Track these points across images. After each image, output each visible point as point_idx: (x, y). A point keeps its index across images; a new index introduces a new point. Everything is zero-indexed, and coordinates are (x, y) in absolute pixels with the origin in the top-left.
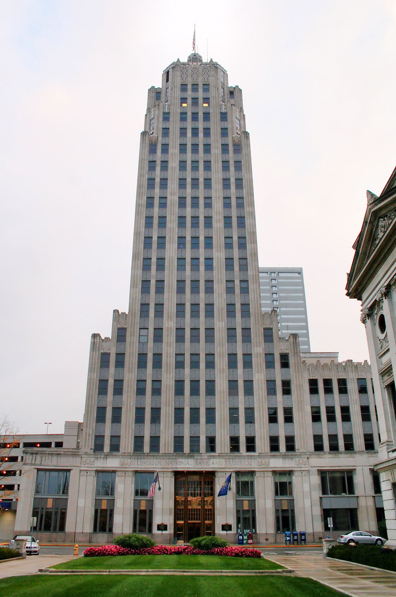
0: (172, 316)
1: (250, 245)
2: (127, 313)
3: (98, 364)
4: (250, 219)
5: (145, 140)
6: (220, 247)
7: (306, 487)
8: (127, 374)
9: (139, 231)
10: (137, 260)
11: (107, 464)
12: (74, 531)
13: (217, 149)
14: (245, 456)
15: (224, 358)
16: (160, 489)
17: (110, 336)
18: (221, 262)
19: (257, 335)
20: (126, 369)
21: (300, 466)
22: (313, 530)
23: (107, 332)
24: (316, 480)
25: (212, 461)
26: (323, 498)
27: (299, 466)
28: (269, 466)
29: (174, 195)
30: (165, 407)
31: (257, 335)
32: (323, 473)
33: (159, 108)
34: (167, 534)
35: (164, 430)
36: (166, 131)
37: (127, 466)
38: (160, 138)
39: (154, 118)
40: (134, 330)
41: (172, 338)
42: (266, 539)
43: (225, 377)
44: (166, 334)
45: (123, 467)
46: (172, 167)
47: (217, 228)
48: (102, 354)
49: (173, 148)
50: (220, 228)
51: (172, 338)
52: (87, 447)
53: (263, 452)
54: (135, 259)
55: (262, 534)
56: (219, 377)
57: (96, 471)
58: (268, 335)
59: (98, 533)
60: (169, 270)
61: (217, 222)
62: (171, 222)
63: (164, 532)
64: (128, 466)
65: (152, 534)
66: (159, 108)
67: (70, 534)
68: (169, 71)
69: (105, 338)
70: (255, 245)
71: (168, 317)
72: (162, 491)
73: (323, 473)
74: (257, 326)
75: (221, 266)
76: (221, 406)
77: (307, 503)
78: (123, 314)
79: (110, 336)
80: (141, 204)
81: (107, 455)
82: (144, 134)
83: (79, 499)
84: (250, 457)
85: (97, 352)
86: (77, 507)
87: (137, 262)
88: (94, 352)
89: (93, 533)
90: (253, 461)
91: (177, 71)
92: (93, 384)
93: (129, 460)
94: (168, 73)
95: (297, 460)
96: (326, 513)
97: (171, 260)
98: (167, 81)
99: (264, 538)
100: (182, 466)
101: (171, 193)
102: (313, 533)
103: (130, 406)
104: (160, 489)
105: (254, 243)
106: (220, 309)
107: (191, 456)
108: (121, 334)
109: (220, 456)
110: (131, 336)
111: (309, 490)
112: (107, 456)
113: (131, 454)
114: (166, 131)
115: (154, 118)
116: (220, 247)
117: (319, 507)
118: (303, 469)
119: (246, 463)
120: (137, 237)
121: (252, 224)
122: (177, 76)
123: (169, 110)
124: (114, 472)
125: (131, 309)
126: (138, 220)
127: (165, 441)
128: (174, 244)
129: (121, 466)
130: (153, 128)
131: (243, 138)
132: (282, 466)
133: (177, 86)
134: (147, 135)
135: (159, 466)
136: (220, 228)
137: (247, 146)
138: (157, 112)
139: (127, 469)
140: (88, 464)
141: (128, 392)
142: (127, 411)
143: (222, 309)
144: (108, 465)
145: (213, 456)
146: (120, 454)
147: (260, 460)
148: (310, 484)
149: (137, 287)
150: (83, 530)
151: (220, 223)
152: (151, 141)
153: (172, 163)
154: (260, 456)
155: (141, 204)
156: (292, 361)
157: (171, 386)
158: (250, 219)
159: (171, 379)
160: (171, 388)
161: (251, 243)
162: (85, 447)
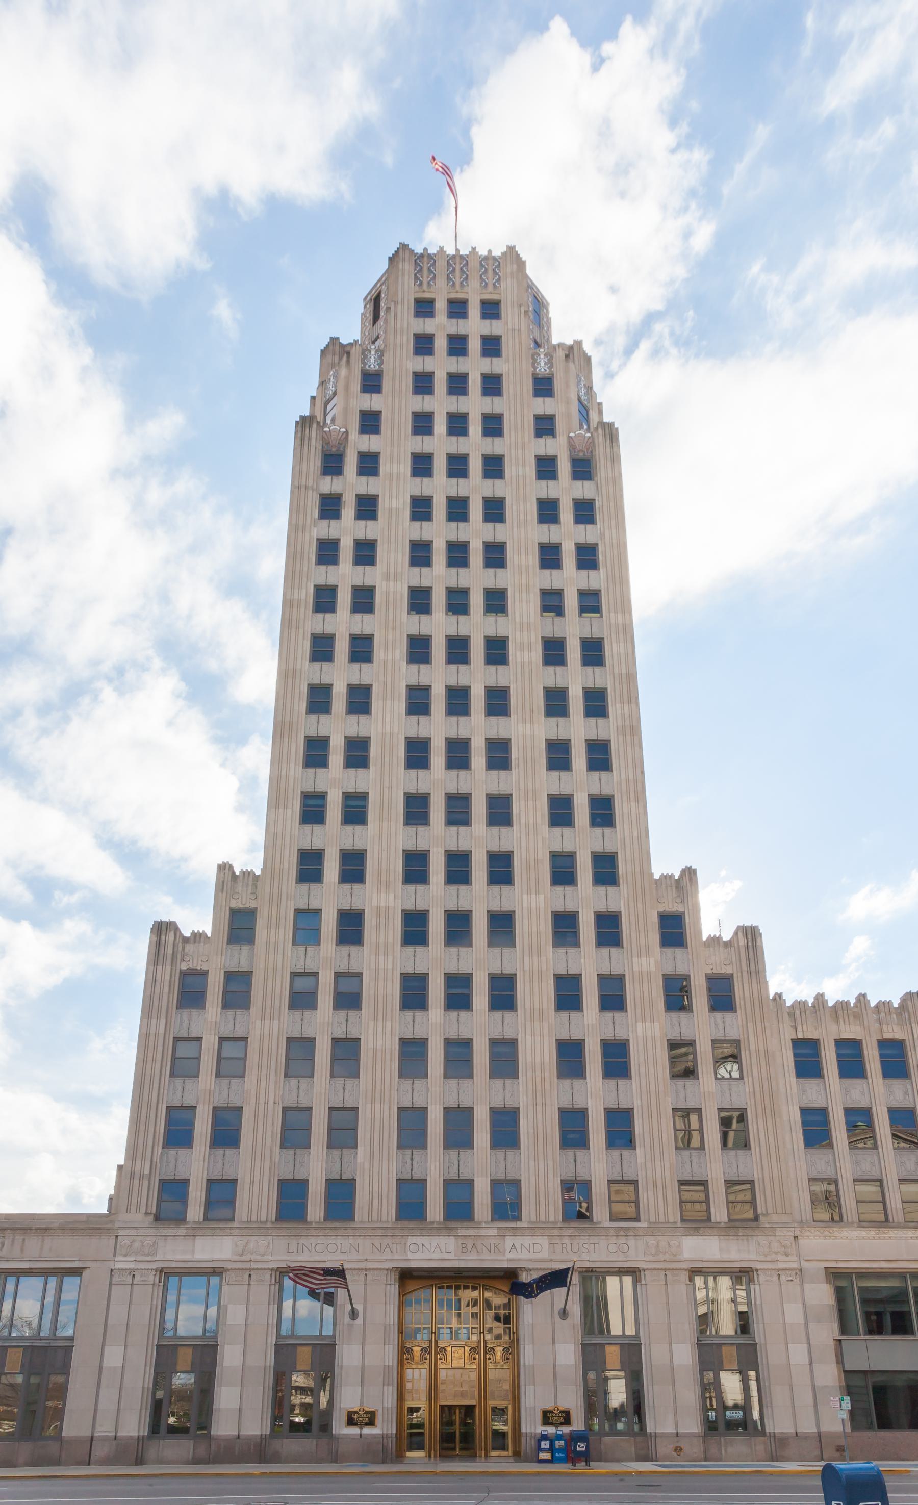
0: (392, 879)
1: (618, 705)
2: (258, 873)
3: (169, 995)
4: (618, 642)
5: (310, 439)
6: (532, 711)
7: (794, 1314)
8: (258, 1023)
9: (291, 666)
10: (286, 739)
11: (193, 1251)
12: (88, 1434)
13: (524, 465)
14: (607, 1229)
15: (544, 984)
16: (354, 1314)
17: (206, 926)
18: (533, 748)
19: (640, 930)
20: (255, 1009)
21: (774, 1257)
22: (818, 1426)
23: (198, 918)
24: (822, 1295)
25: (509, 1241)
26: (843, 1342)
27: (769, 1258)
28: (678, 1257)
29: (395, 580)
30: (369, 1106)
31: (640, 930)
32: (839, 1278)
33: (348, 361)
34: (375, 1436)
35: (367, 1165)
36: (370, 422)
37: (254, 1257)
38: (354, 436)
39: (335, 394)
40: (279, 912)
41: (391, 933)
42: (676, 1450)
43: (546, 1031)
44: (374, 923)
45: (243, 1258)
46: (390, 510)
47: (523, 664)
48: (184, 974)
49: (392, 461)
50: (530, 663)
51: (391, 933)
52: (133, 1208)
53: (662, 1219)
54: (282, 736)
55: (664, 1435)
56: (528, 1031)
57: (161, 1270)
58: (674, 930)
59: (164, 1438)
60: (383, 766)
61: (522, 649)
62: (386, 648)
63: (367, 1431)
64: (259, 1258)
65: (331, 1436)
66: (348, 361)
67: (77, 1441)
68: (379, 295)
69: (193, 933)
70: (633, 706)
71: (380, 882)
72: (359, 1321)
73: (839, 1278)
74: (640, 906)
75: (533, 759)
76: (535, 1105)
77: (798, 1354)
78: (247, 874)
79: (206, 926)
80: (299, 601)
81: (194, 1228)
82: (304, 423)
83: (107, 1348)
84: (622, 1233)
85: (168, 968)
86: (101, 1368)
87: (285, 744)
88: (160, 968)
89: (149, 1437)
90: (632, 1242)
91: (404, 260)
92: (155, 1048)
93: (263, 1242)
94: (377, 300)
95: (763, 1241)
96: (854, 1382)
97: (297, 581)
98: (376, 318)
99: (671, 1447)
100: (418, 1256)
101: (388, 574)
102: (819, 1434)
103: (266, 1103)
104: (354, 1314)
105: (630, 702)
106: (532, 863)
107: (447, 1229)
108: (239, 925)
109: (533, 1229)
110: (269, 927)
111: (802, 1321)
112: (196, 1230)
113: (269, 1225)
114: (370, 422)
115: (335, 394)
116: (532, 711)
117: (834, 1365)
118: (781, 1265)
119: (612, 1248)
120: (286, 687)
121: (626, 655)
122: (403, 275)
123: (380, 364)
124: (217, 1272)
125: (269, 866)
126: (289, 641)
127: (371, 1193)
128: (396, 703)
129: (237, 1258)
130: (333, 420)
131: (600, 438)
132: (717, 1256)
133: (403, 299)
134: (315, 426)
135: (354, 1256)
136: (530, 663)
137: (613, 460)
138: (343, 372)
139: (254, 1265)
140: (136, 1253)
141: (260, 1067)
142: (256, 1116)
143: (537, 862)
144: (198, 1256)
145: (515, 1229)
146: (236, 1224)
147: (652, 1241)
148: (804, 1304)
149: (286, 807)
150: (116, 1432)
151: (530, 650)
152: (326, 442)
153: (391, 497)
154: (654, 1229)
155: (299, 601)
156: (741, 992)
157: (388, 1052)
158: (618, 642)
159: (388, 1036)
160: (388, 1057)
161: (622, 702)
162: (128, 1210)
